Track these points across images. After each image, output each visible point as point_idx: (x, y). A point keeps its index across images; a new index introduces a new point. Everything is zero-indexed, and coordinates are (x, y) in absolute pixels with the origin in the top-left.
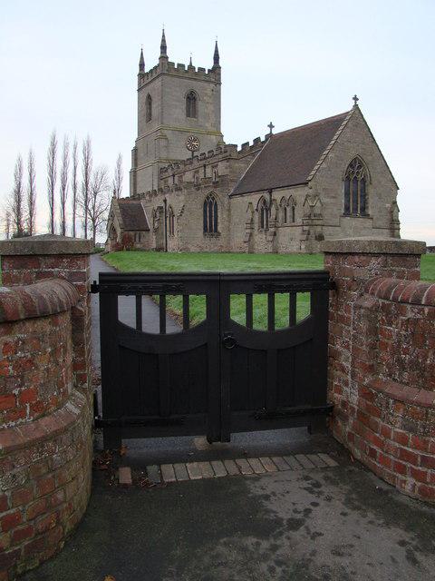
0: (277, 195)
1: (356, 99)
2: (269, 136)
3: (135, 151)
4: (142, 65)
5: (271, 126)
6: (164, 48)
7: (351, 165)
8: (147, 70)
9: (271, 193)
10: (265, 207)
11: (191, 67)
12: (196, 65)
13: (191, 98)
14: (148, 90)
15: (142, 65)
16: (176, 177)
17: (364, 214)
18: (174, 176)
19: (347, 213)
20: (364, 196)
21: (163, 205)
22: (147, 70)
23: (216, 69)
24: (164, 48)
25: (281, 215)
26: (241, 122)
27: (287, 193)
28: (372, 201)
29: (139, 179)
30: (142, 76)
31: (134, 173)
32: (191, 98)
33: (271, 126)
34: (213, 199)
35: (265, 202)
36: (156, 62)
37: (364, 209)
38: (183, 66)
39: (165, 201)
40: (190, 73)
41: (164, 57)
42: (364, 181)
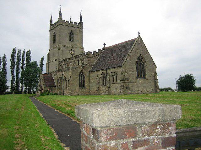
0: (109, 71)
1: (139, 33)
2: (104, 48)
3: (49, 54)
4: (51, 21)
5: (105, 44)
6: (60, 14)
7: (138, 59)
8: (53, 23)
9: (107, 71)
10: (105, 76)
11: (71, 22)
12: (73, 21)
13: (71, 34)
14: (54, 31)
15: (51, 21)
16: (66, 65)
17: (145, 79)
18: (65, 64)
19: (138, 77)
20: (144, 70)
21: (62, 76)
22: (53, 23)
23: (81, 23)
24: (60, 14)
25: (111, 79)
26: (92, 42)
27: (114, 70)
28: (147, 72)
29: (50, 66)
30: (51, 25)
31: (48, 64)
32: (71, 34)
33: (105, 44)
34: (83, 73)
35: (104, 74)
36: (57, 20)
37: (144, 76)
38: (76, 23)
39: (63, 75)
40: (70, 24)
41: (60, 18)
42: (143, 65)
